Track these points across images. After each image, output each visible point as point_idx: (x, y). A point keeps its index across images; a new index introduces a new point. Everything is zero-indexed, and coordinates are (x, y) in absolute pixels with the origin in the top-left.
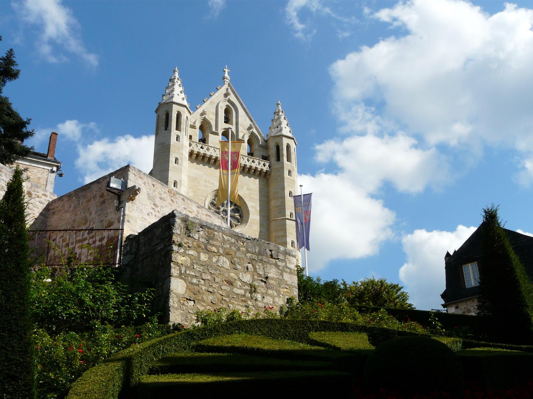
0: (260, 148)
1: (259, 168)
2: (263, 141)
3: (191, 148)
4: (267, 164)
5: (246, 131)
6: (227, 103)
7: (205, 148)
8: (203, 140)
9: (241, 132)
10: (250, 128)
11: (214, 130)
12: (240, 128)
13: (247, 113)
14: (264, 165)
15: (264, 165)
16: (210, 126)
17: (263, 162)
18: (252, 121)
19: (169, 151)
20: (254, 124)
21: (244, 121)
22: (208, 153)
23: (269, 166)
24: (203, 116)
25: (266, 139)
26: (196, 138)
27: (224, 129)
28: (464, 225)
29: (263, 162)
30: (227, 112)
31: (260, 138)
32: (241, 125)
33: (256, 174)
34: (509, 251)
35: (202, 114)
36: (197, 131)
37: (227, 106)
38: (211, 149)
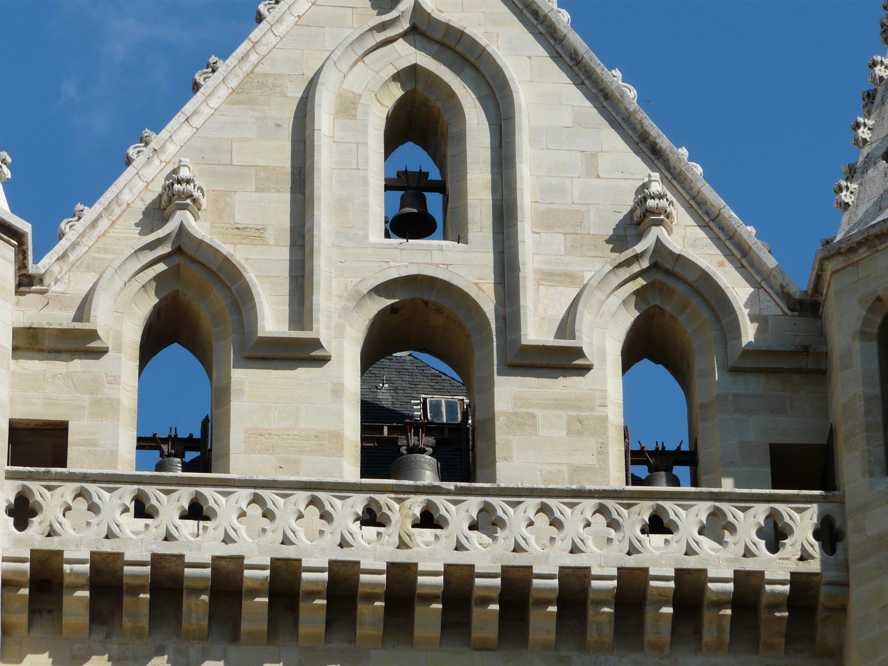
0: (754, 385)
1: (719, 563)
2: (773, 308)
3: (34, 536)
4: (803, 522)
5: (597, 264)
6: (406, 54)
7: (226, 506)
8: (188, 449)
9: (549, 277)
10: (640, 219)
11: (272, 319)
12: (533, 249)
13: (603, 99)
14: (775, 534)
15: (775, 534)
16: (241, 299)
17: (760, 512)
18: (652, 153)
19: (413, 623)
20: (675, 177)
21: (568, 172)
22: (257, 550)
23: (828, 534)
24: (171, 227)
25: (800, 285)
26: (107, 438)
27: (382, 290)
28: (638, 317)
29: (760, 512)
30: (418, 121)
31: (738, 290)
32: (548, 221)
33: (708, 635)
34: (680, 160)
35: (157, 212)
36: (121, 370)
37: (410, 76)
38: (518, 518)
